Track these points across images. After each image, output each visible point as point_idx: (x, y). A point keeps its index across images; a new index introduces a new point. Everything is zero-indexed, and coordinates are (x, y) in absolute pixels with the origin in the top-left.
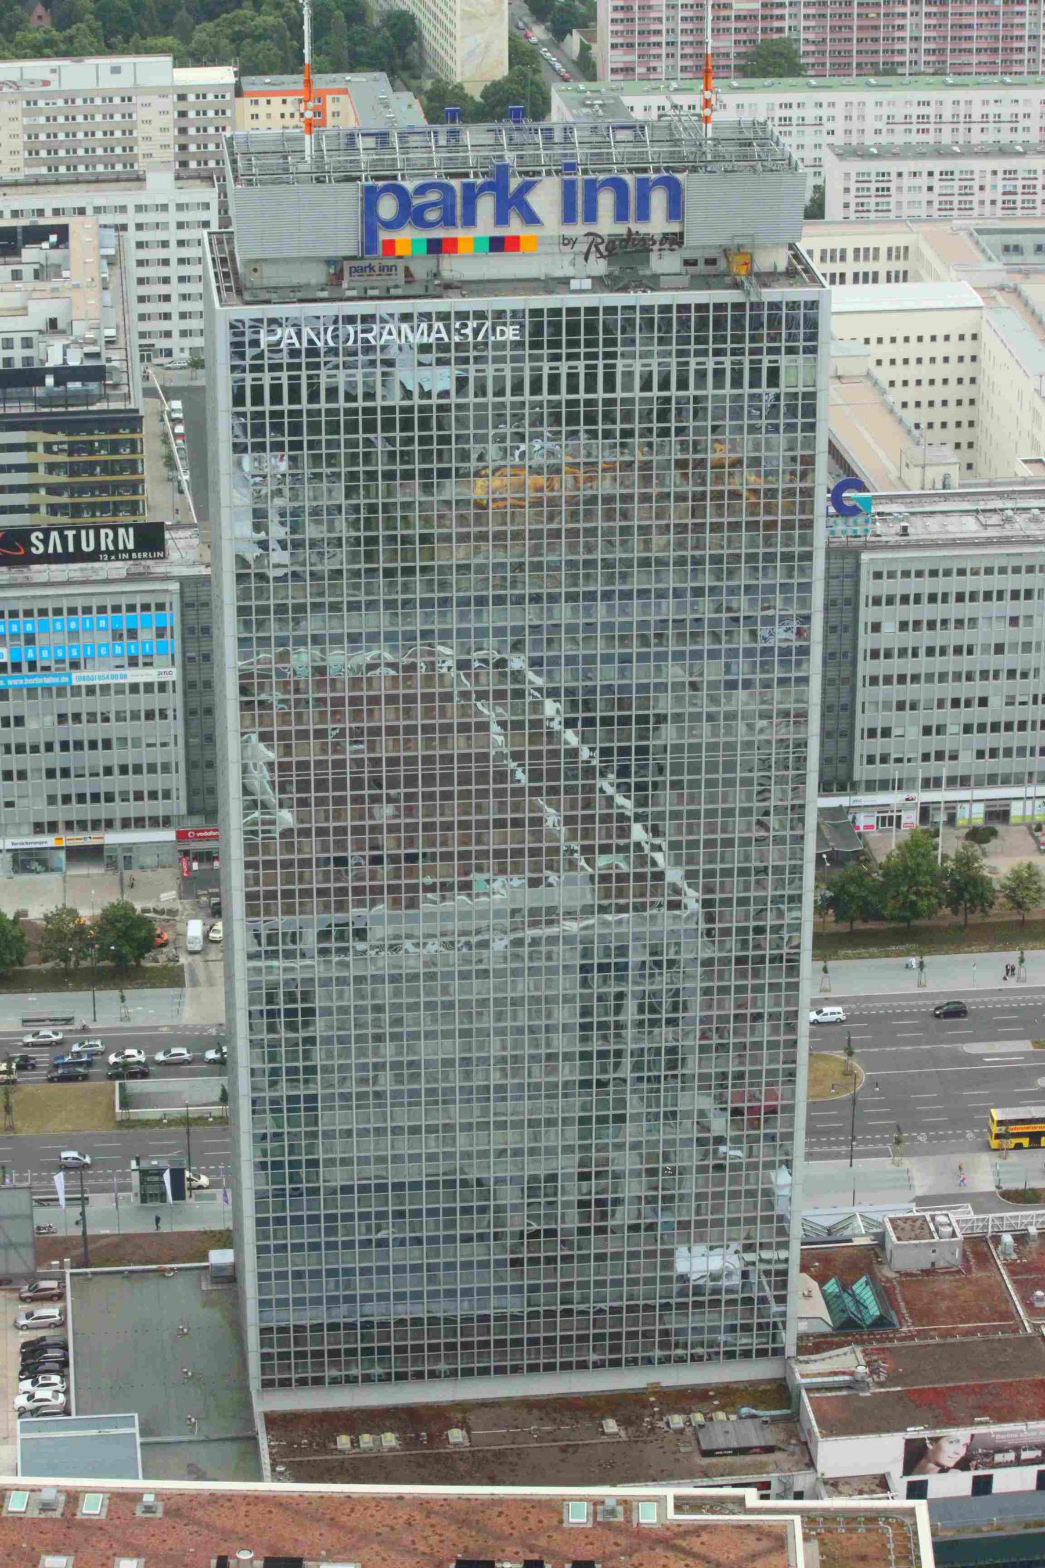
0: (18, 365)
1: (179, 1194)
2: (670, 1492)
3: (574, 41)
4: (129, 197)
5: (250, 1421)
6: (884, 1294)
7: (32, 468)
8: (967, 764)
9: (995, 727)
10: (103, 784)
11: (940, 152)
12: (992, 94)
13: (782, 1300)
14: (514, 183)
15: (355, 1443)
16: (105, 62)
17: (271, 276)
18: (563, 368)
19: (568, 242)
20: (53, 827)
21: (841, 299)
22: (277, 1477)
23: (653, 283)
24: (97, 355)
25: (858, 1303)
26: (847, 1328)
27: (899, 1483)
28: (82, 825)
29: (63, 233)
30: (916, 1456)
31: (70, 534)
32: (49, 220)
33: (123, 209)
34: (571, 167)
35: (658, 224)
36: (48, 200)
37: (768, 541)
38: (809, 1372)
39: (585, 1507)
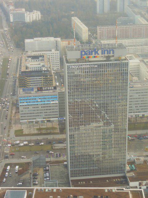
0: (33, 70)
1: (60, 156)
2: (116, 188)
3: (95, 35)
4: (50, 52)
5: (69, 181)
6: (135, 166)
7: (42, 81)
8: (140, 110)
9: (24, 114)
10: (51, 114)
11: (135, 46)
12: (139, 40)
13: (125, 167)
14: (96, 50)
15: (80, 183)
16: (47, 38)
17: (72, 60)
18: (102, 70)
19: (102, 56)
20: (45, 118)
21: (130, 61)
22: (72, 187)
23: (111, 61)
24: (48, 69)
25: (132, 167)
26: (132, 170)
27: (138, 187)
28: (48, 118)
29: (43, 56)
30: (140, 184)
31: (47, 88)
32: (42, 55)
33: (49, 54)
34: (102, 49)
35: (111, 54)
36: (42, 53)
37: (97, 89)
38: (128, 175)
39: (107, 190)
